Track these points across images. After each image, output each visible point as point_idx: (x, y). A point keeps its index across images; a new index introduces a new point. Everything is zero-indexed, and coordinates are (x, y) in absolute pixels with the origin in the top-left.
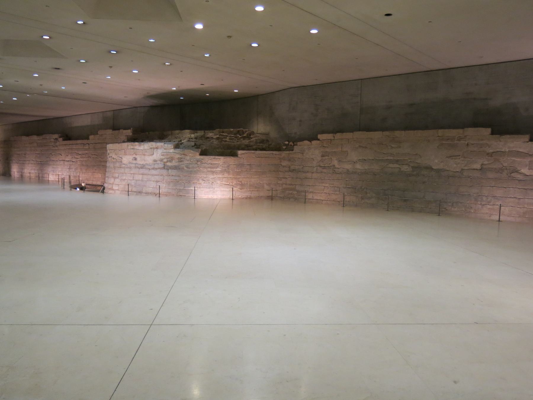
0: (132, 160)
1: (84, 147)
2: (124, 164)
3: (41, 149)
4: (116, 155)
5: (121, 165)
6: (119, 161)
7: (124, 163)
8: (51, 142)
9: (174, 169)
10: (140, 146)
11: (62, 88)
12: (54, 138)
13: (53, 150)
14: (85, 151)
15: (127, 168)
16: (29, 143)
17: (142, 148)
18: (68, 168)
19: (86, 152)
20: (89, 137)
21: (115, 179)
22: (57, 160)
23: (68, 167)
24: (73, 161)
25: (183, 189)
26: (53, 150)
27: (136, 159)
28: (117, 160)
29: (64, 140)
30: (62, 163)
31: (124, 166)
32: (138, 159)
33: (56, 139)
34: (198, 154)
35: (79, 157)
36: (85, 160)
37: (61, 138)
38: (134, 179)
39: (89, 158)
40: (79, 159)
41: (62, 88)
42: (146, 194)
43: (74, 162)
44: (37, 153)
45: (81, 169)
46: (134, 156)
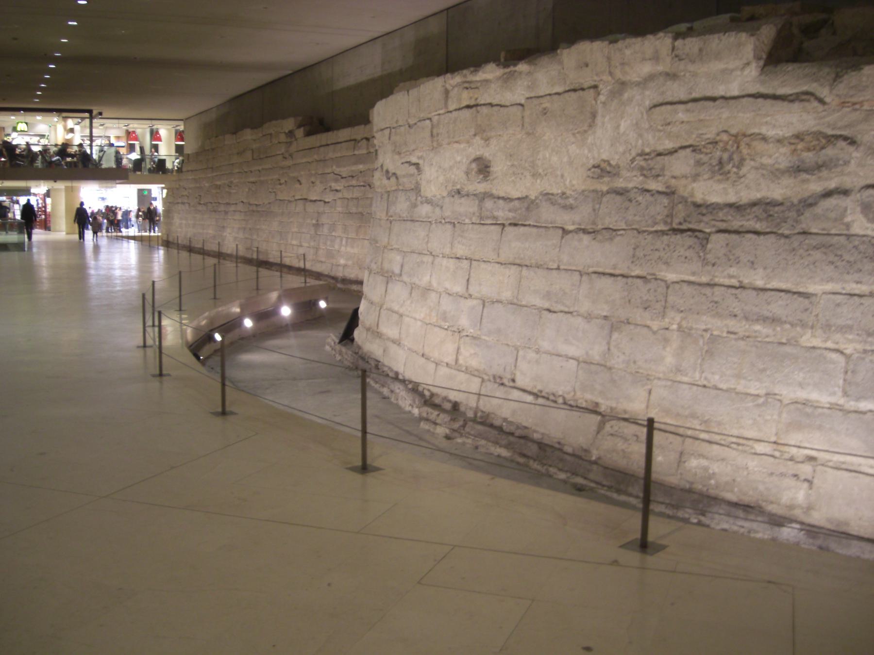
1: (356, 152)
2: (429, 201)
3: (260, 168)
4: (399, 153)
5: (415, 206)
8: (279, 143)
9: (757, 233)
10: (507, 80)
12: (287, 131)
13: (282, 168)
14: (356, 163)
15: (442, 221)
16: (238, 154)
17: (518, 93)
18: (314, 225)
19: (361, 167)
21: (390, 285)
22: (291, 199)
23: (314, 222)
24: (325, 202)
25: (833, 407)
26: (282, 168)
27: (483, 168)
28: (401, 180)
29: (308, 134)
30: (300, 206)
31: (424, 210)
32: (499, 167)
33: (291, 134)
35: (342, 188)
36: (354, 197)
37: (302, 129)
38: (473, 290)
39: (368, 187)
40: (340, 195)
42: (536, 396)
43: (328, 202)
44: (252, 180)
45: (345, 229)
46: (477, 148)
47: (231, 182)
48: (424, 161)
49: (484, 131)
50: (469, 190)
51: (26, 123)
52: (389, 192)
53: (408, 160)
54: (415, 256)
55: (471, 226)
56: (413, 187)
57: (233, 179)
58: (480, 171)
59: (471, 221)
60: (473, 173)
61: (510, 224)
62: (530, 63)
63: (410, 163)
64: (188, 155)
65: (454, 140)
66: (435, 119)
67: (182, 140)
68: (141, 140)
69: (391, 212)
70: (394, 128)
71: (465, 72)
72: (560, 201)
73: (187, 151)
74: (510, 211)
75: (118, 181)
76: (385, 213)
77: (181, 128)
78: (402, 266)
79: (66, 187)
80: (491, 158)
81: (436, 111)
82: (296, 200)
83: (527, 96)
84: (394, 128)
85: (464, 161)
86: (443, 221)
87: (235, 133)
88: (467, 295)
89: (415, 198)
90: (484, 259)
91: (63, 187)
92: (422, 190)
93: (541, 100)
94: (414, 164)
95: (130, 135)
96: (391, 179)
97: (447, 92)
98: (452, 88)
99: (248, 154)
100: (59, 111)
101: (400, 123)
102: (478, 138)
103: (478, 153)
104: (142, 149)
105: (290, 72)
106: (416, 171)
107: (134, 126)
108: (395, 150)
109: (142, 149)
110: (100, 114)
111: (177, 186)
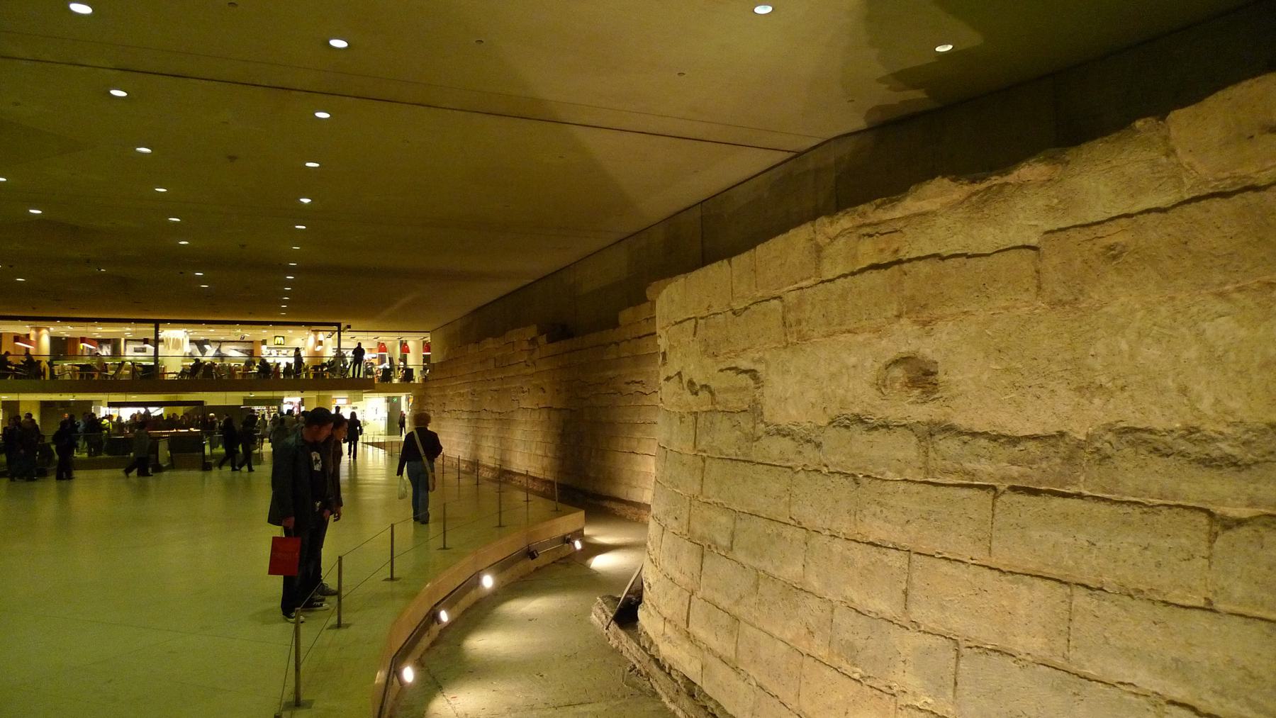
0: (881, 385)
2: (781, 433)
6: (734, 402)
7: (783, 422)
8: (522, 350)
11: (32, 211)
12: (529, 339)
20: (617, 317)
28: (719, 397)
31: (777, 448)
34: (530, 560)
41: (32, 211)
44: (494, 388)
47: (474, 390)
48: (768, 366)
49: (925, 307)
50: (887, 418)
51: (283, 337)
52: (696, 413)
53: (733, 365)
54: (761, 522)
55: (903, 486)
56: (746, 407)
57: (475, 388)
58: (913, 383)
59: (901, 476)
60: (897, 385)
61: (1014, 489)
62: (1052, 160)
63: (739, 371)
64: (434, 364)
65: (844, 328)
66: (791, 298)
67: (428, 350)
68: (390, 352)
69: (703, 444)
70: (702, 318)
71: (861, 208)
72: (1184, 446)
73: (433, 361)
74: (1013, 462)
75: (364, 391)
76: (691, 444)
77: (428, 339)
78: (733, 535)
79: (318, 396)
80: (937, 357)
81: (796, 283)
82: (539, 408)
83: (1047, 228)
84: (702, 318)
85: (868, 364)
86: (825, 470)
87: (477, 342)
88: (904, 621)
89: (751, 425)
90: (946, 555)
91: (315, 396)
92: (766, 414)
93: (1100, 231)
94: (746, 372)
95: (382, 347)
96: (700, 393)
97: (819, 250)
98: (828, 241)
99: (491, 364)
100: (307, 324)
101: (715, 309)
102: (904, 321)
103: (904, 349)
104: (391, 360)
105: (532, 281)
106: (751, 383)
107: (386, 338)
108: (706, 351)
109: (391, 360)
110: (349, 327)
111: (423, 394)
